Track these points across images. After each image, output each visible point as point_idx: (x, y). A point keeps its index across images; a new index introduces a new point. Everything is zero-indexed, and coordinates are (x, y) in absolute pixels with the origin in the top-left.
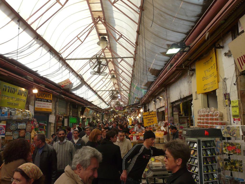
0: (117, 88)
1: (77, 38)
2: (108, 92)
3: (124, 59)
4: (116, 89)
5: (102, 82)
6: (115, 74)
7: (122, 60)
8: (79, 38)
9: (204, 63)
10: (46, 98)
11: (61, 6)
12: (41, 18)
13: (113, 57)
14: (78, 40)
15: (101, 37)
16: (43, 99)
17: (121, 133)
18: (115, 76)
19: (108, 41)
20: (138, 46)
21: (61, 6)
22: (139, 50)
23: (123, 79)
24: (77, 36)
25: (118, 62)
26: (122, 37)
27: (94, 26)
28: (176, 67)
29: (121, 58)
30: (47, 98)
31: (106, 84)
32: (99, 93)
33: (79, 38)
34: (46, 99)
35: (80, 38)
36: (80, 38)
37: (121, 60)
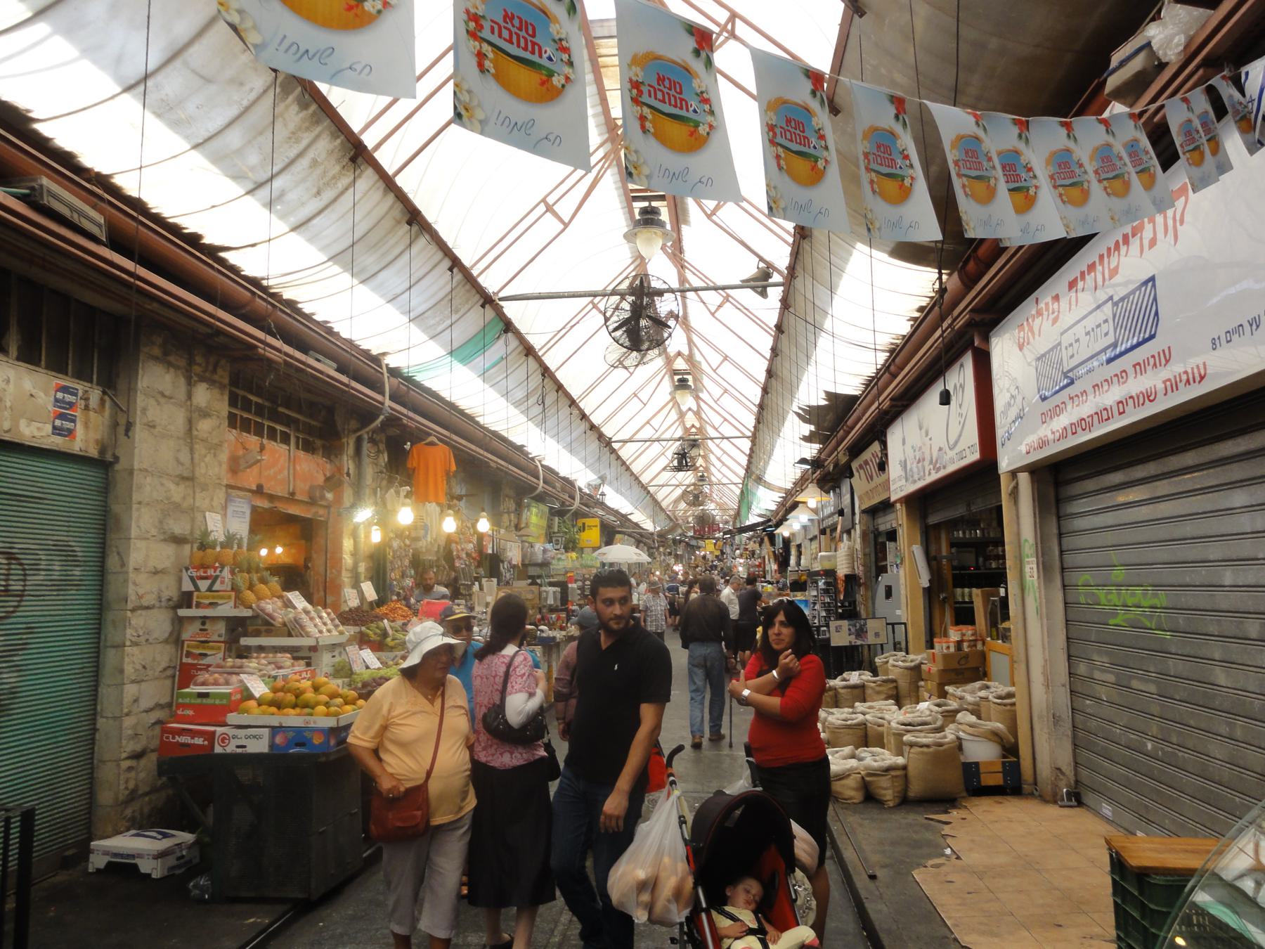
0: (679, 354)
1: (542, 208)
5: (635, 404)
6: (689, 374)
7: (727, 299)
8: (549, 209)
9: (380, 760)
11: (562, 227)
14: (548, 214)
15: (676, 378)
17: (1124, 104)
18: (691, 383)
19: (668, 227)
20: (779, 358)
21: (562, 227)
24: (544, 200)
26: (728, 301)
28: (971, 311)
31: (642, 387)
32: (626, 452)
33: (549, 209)
35: (555, 207)
36: (555, 207)
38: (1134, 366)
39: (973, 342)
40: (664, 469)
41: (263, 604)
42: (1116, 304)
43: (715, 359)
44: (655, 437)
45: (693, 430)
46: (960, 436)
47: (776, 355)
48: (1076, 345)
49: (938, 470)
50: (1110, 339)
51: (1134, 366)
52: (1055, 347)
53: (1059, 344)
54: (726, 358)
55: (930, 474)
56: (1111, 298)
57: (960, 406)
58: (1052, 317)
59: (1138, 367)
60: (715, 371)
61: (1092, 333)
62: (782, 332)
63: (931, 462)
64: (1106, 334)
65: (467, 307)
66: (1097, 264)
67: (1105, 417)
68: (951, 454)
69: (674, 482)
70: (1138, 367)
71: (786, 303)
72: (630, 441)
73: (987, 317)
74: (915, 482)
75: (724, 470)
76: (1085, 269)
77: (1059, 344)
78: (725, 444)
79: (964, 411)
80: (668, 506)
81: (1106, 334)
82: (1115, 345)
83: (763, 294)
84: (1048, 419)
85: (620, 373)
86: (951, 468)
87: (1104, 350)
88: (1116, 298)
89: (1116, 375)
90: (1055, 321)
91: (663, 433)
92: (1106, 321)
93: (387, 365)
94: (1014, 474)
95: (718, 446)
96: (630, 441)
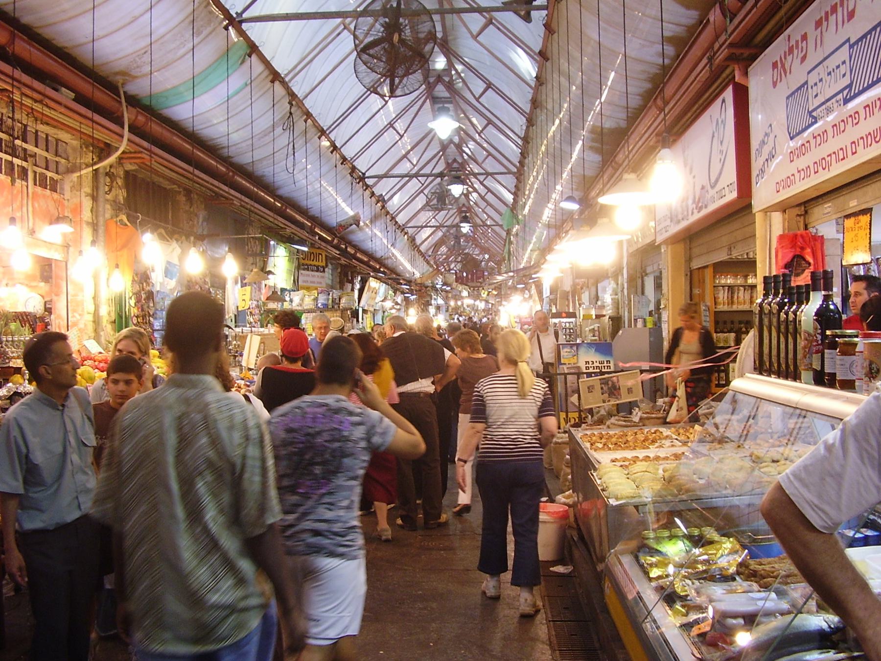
2: (414, 185)
3: (496, 20)
4: (462, 208)
5: (390, 137)
7: (490, 22)
10: (315, 263)
12: (368, 163)
13: (446, 6)
16: (311, 265)
22: (556, 90)
23: (490, 122)
25: (471, 33)
26: (492, 23)
27: (441, 153)
29: (480, 10)
30: (317, 263)
34: (315, 266)
37: (484, 20)
38: (865, 108)
39: (734, 77)
40: (422, 209)
41: (111, 349)
42: (851, 46)
43: (478, 86)
44: (414, 172)
45: (455, 165)
46: (720, 174)
47: (541, 84)
48: (819, 85)
49: (700, 209)
50: (846, 81)
51: (865, 108)
52: (803, 86)
53: (806, 83)
54: (489, 86)
55: (692, 213)
56: (848, 40)
57: (721, 142)
58: (801, 55)
59: (835, 128)
60: (477, 100)
61: (832, 73)
62: (547, 59)
63: (694, 202)
64: (844, 75)
65: (209, 29)
66: (838, 6)
67: (841, 157)
68: (712, 192)
69: (433, 223)
70: (867, 109)
71: (549, 28)
72: (386, 176)
73: (746, 52)
74: (679, 222)
75: (489, 210)
76: (799, 38)
77: (806, 83)
78: (490, 182)
79: (724, 148)
80: (427, 250)
81: (844, 75)
82: (850, 86)
83: (527, 18)
84: (795, 157)
85: (375, 101)
86: (712, 207)
87: (841, 91)
88: (852, 41)
89: (851, 116)
90: (804, 59)
91: (421, 169)
92: (844, 62)
93: (125, 93)
94: (766, 211)
95: (481, 183)
96: (386, 176)
